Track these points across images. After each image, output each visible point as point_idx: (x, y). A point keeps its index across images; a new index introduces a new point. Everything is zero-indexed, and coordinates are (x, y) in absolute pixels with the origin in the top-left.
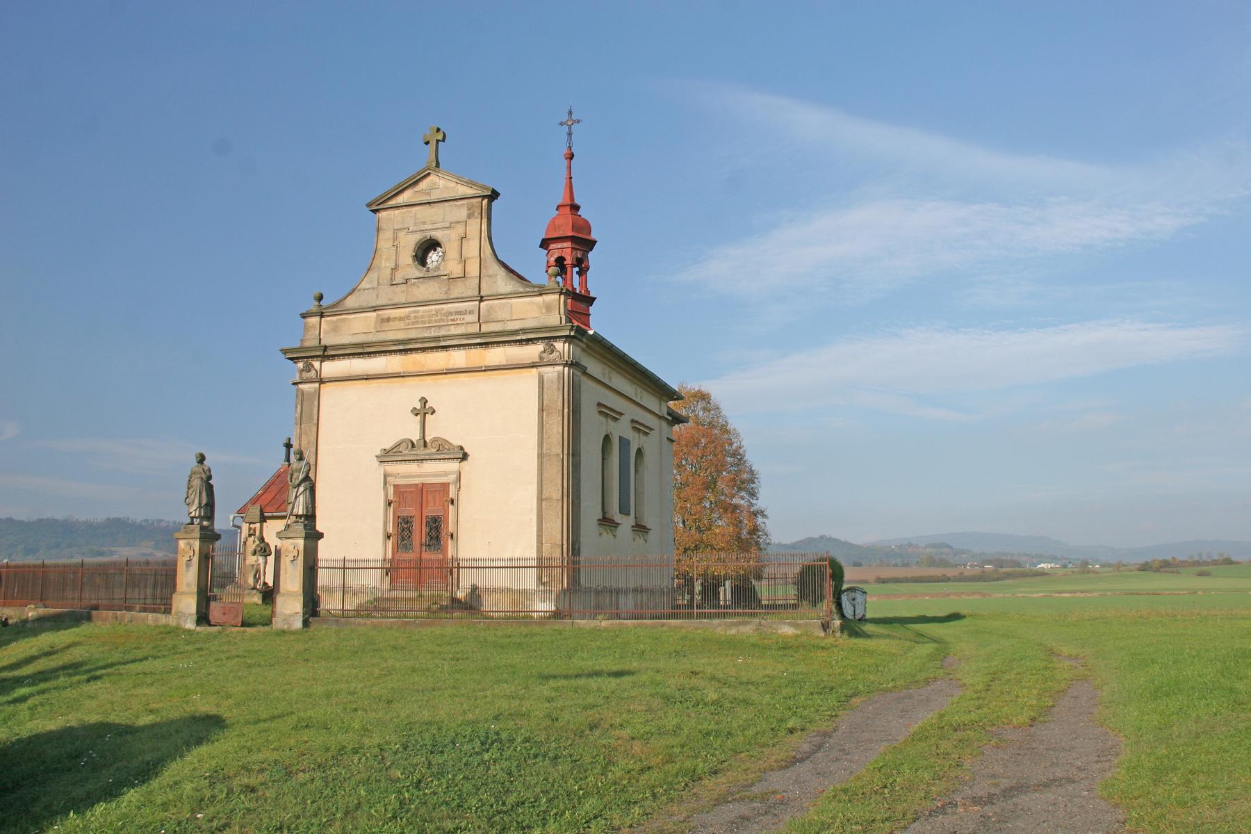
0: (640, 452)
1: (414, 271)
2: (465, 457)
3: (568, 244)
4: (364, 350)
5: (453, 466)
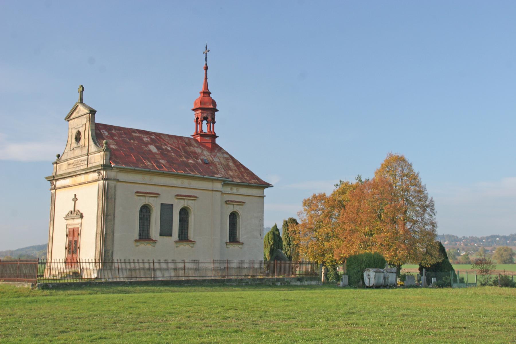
0: (184, 213)
1: (74, 145)
2: (82, 217)
3: (199, 111)
4: (70, 175)
5: (79, 221)
